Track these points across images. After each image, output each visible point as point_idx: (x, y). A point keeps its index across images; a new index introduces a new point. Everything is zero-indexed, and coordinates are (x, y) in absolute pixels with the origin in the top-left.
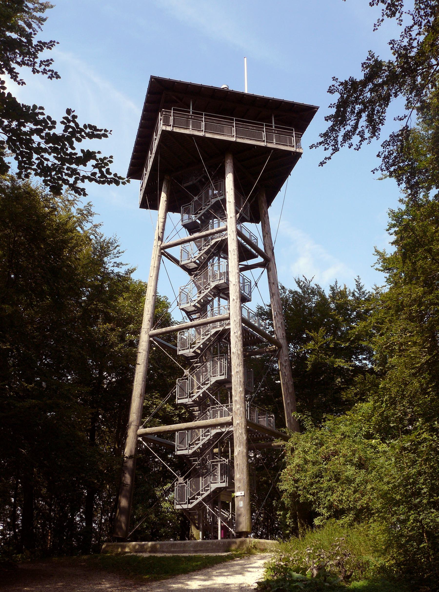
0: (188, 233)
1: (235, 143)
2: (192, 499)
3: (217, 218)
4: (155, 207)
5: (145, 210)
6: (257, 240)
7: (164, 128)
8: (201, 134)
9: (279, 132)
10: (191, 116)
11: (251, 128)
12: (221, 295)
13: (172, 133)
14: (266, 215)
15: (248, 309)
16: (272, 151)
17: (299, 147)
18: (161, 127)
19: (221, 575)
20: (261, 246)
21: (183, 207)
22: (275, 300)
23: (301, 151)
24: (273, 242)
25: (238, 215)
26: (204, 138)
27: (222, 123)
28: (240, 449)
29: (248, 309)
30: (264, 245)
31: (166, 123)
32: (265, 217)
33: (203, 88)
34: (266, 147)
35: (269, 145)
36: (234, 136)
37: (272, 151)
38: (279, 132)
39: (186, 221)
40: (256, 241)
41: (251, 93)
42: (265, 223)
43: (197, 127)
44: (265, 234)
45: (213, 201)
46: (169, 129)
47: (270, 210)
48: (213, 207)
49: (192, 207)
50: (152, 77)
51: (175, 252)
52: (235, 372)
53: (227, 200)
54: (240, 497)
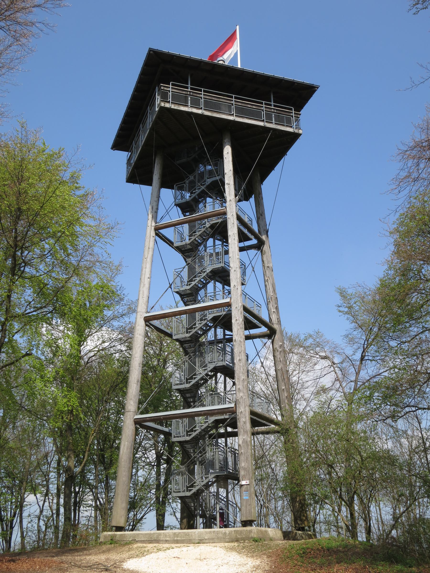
0: (180, 212)
1: (234, 122)
2: (190, 487)
3: (211, 198)
4: (149, 182)
5: (131, 184)
6: (251, 221)
7: (163, 104)
8: (200, 112)
9: (278, 112)
10: (190, 92)
11: (251, 105)
12: (217, 278)
13: (169, 110)
14: (260, 196)
15: (245, 294)
16: (271, 131)
17: (298, 127)
18: (159, 102)
19: (96, 554)
20: (255, 227)
21: (176, 185)
22: (270, 284)
23: (301, 132)
24: (268, 224)
25: (237, 197)
26: (202, 116)
27: (221, 100)
28: (244, 438)
29: (245, 294)
30: (259, 226)
31: (165, 98)
32: (259, 197)
33: (202, 63)
34: (264, 128)
35: (268, 125)
36: (233, 114)
37: (271, 131)
38: (278, 112)
39: (179, 201)
40: (250, 222)
41: (249, 68)
42: (259, 204)
43: (196, 104)
44: (259, 215)
45: (209, 181)
46: (167, 105)
47: (262, 187)
48: (208, 187)
49: (186, 185)
50: (150, 50)
51: (168, 233)
52: (238, 360)
53: (226, 182)
54: (245, 486)
